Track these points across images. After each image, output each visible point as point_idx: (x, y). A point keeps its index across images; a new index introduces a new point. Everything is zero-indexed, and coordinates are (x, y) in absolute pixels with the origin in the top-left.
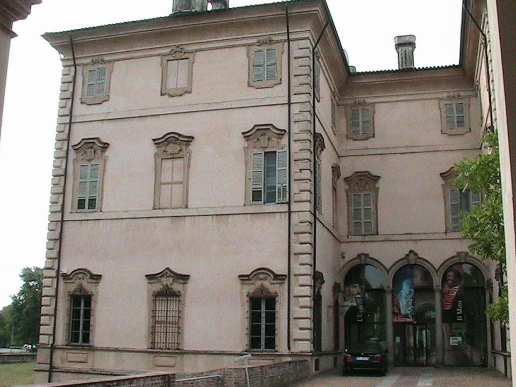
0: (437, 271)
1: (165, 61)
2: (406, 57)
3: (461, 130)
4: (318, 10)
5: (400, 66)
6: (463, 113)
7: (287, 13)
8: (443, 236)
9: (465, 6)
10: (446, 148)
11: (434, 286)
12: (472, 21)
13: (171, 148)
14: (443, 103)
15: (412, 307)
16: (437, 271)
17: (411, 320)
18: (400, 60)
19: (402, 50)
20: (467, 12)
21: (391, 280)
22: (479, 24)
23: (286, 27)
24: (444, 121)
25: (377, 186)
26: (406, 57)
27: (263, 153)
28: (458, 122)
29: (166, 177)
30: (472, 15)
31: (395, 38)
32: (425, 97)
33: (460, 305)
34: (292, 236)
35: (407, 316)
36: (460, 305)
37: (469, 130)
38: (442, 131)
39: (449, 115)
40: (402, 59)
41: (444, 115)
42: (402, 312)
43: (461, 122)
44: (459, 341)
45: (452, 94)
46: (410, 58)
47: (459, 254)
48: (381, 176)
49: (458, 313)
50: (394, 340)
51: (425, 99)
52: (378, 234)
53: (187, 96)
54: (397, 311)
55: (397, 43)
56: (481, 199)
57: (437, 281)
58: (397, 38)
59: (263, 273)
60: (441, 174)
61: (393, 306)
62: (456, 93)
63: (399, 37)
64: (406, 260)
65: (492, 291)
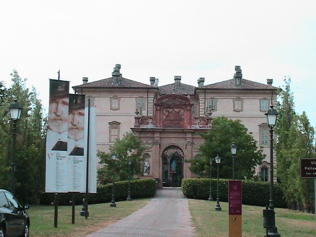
13: (114, 126)
16: (169, 157)
29: (113, 133)
34: (148, 109)
35: (174, 171)
42: (173, 170)
53: (118, 111)
54: (171, 170)
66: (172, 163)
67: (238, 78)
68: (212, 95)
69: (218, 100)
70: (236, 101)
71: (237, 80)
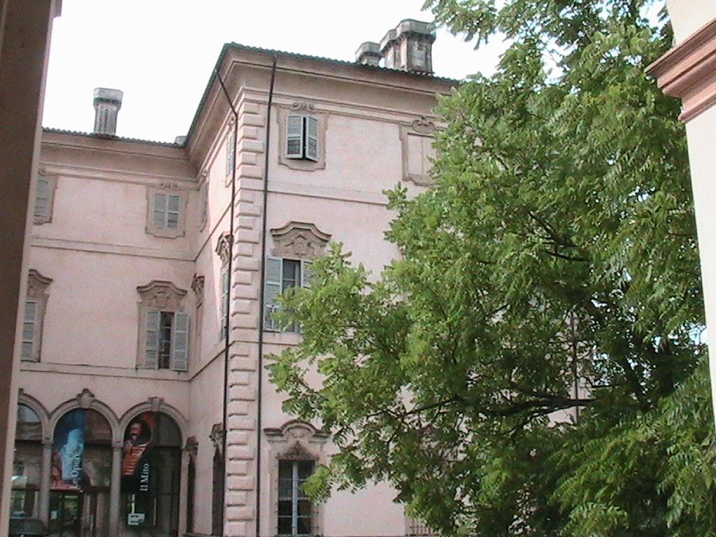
0: (119, 421)
1: (405, 134)
2: (106, 119)
3: (172, 233)
4: (234, 62)
5: (98, 129)
6: (177, 210)
7: (274, 67)
8: (133, 373)
9: (218, 71)
10: (149, 252)
11: (114, 439)
12: (222, 91)
14: (153, 191)
15: (80, 469)
16: (50, 416)
17: (76, 487)
18: (98, 120)
19: (102, 108)
20: (217, 78)
21: (53, 430)
22: (232, 99)
23: (270, 83)
24: (152, 215)
25: (46, 292)
26: (106, 119)
27: (282, 260)
28: (169, 221)
30: (225, 84)
31: (95, 89)
32: (127, 178)
33: (146, 470)
35: (70, 482)
36: (146, 470)
37: (182, 234)
38: (146, 229)
39: (158, 210)
40: (100, 119)
41: (152, 209)
42: (65, 476)
43: (173, 222)
44: (140, 520)
45: (165, 182)
46: (111, 120)
47: (151, 399)
48: (54, 279)
49: (142, 481)
50: (50, 516)
51: (129, 182)
52: (39, 362)
54: (56, 473)
55: (97, 97)
56: (188, 328)
57: (118, 434)
58: (98, 90)
59: (298, 427)
60: (138, 288)
61: (52, 466)
62: (172, 182)
63: (102, 90)
64: (76, 402)
65: (196, 454)
66: (65, 441)
67: (419, 41)
68: (307, 94)
69: (330, 121)
70: (411, 137)
71: (415, 48)
